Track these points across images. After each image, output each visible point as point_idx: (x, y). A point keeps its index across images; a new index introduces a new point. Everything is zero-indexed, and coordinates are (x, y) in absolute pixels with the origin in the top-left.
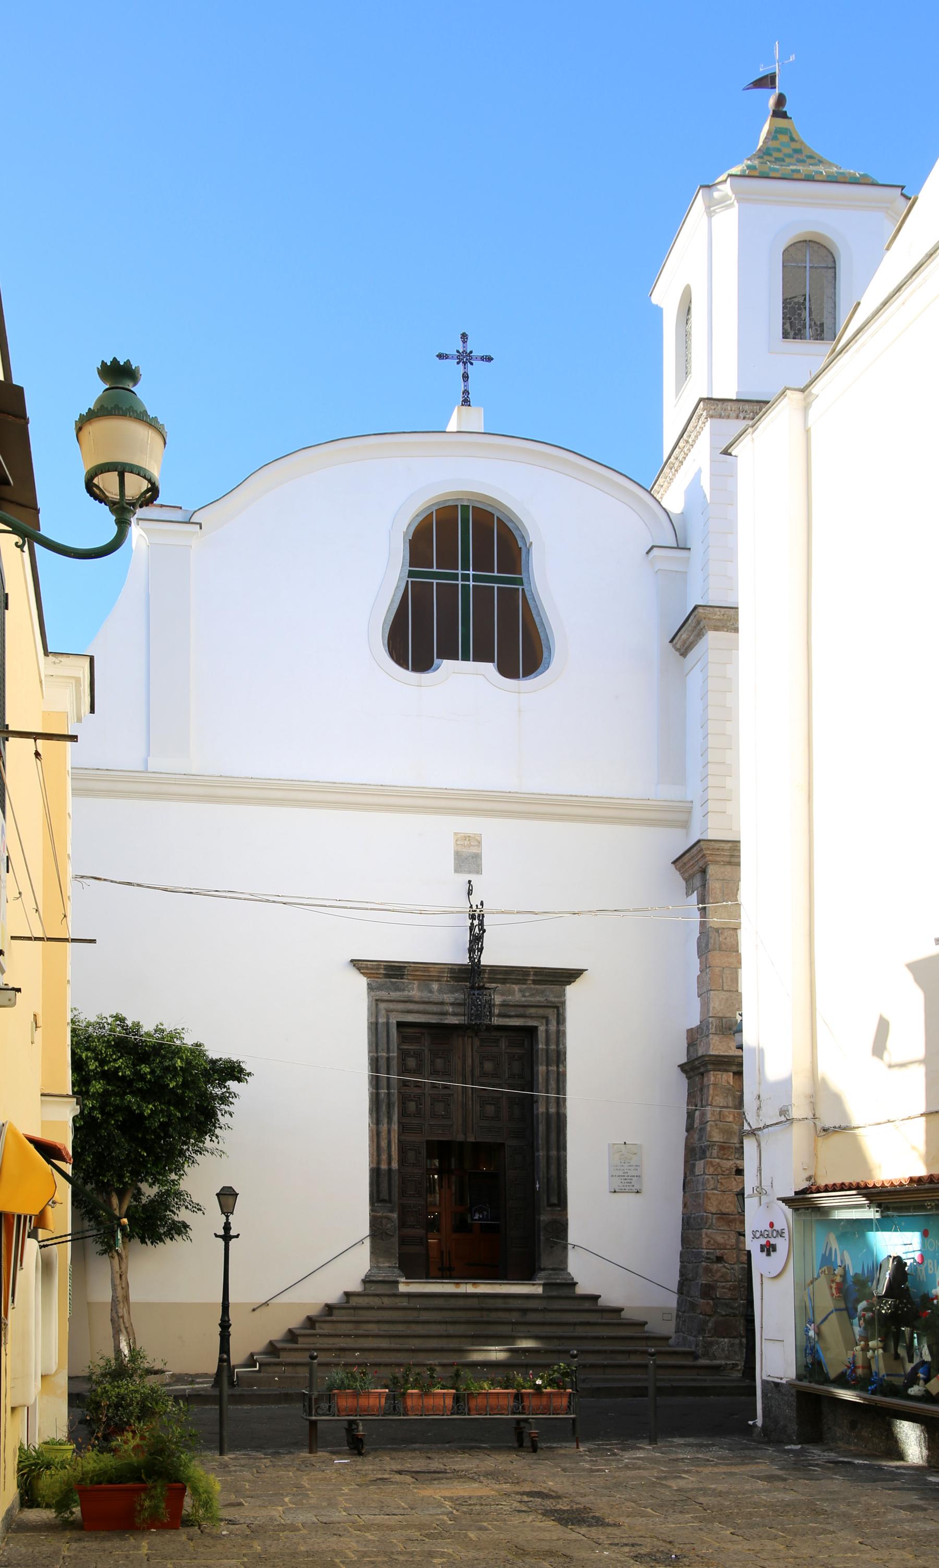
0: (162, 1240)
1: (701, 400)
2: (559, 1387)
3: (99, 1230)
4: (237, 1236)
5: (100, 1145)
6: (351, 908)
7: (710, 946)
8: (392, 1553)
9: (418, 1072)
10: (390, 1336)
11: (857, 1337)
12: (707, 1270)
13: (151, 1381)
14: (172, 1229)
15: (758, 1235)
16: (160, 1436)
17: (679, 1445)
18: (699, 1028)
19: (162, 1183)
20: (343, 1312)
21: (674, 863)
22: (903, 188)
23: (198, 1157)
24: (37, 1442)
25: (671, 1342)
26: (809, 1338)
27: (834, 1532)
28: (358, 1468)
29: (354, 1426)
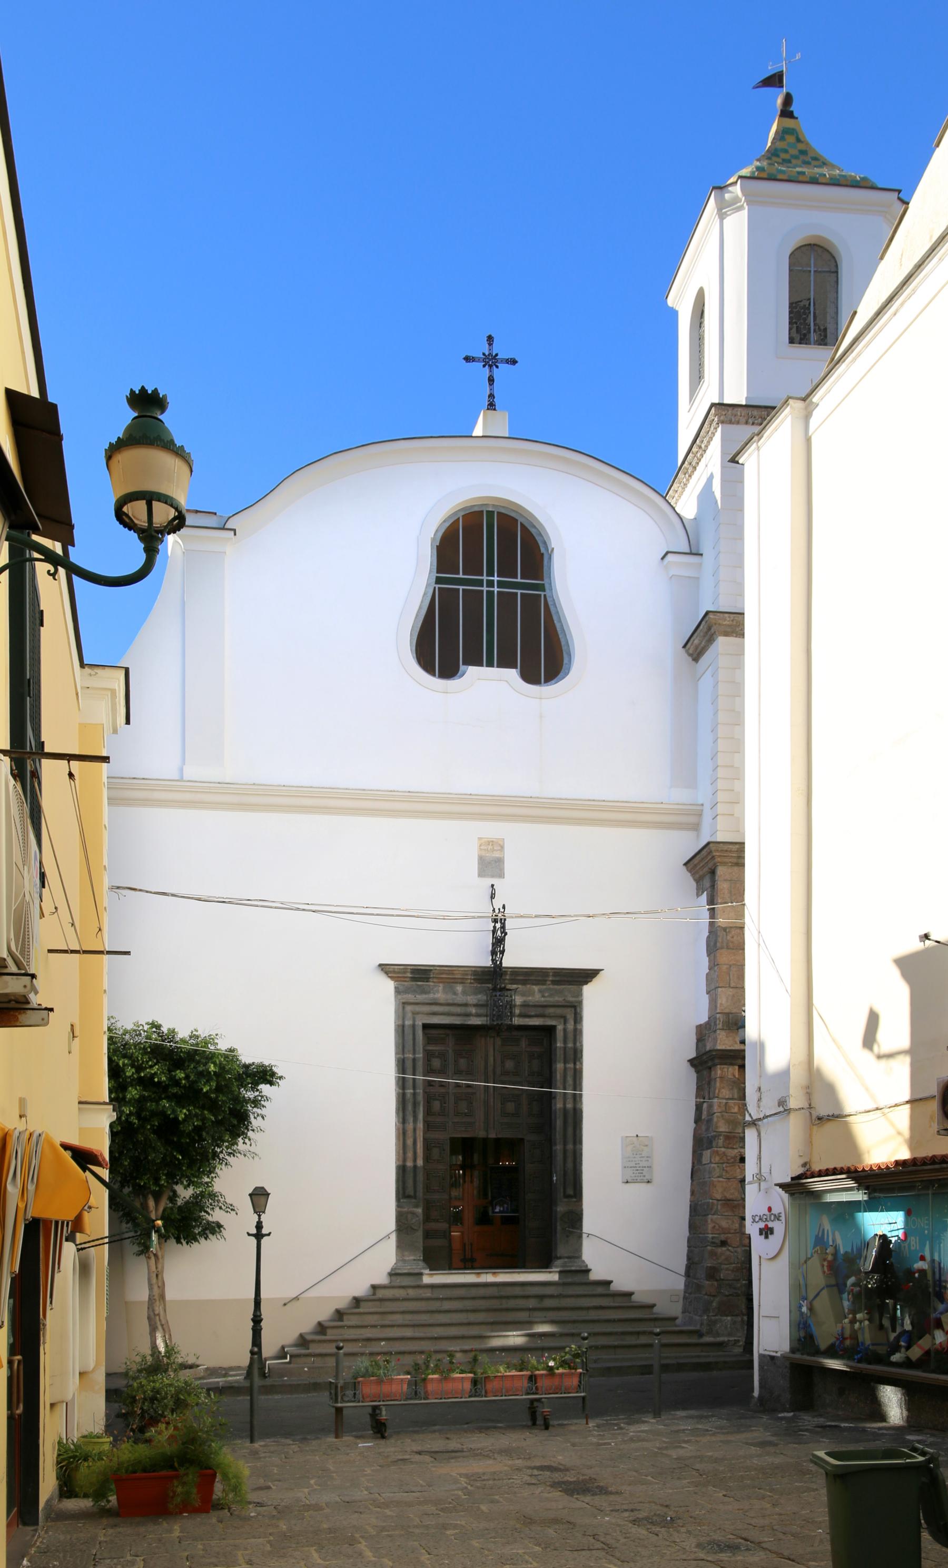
0: (196, 1240)
1: (713, 405)
2: (570, 1368)
3: (136, 1232)
4: (269, 1234)
5: (136, 1150)
6: (377, 915)
7: (718, 945)
8: (409, 1527)
9: (442, 1072)
10: (414, 1326)
11: (846, 1311)
12: (713, 1254)
13: (185, 1375)
14: (206, 1229)
15: (757, 1219)
16: (192, 1427)
17: (682, 1418)
18: (707, 1023)
19: (197, 1185)
20: (370, 1303)
21: (685, 864)
22: (899, 191)
23: (231, 1159)
24: (75, 1436)
25: (678, 1322)
26: (802, 1314)
27: (817, 1490)
28: (382, 1450)
29: (378, 1412)
